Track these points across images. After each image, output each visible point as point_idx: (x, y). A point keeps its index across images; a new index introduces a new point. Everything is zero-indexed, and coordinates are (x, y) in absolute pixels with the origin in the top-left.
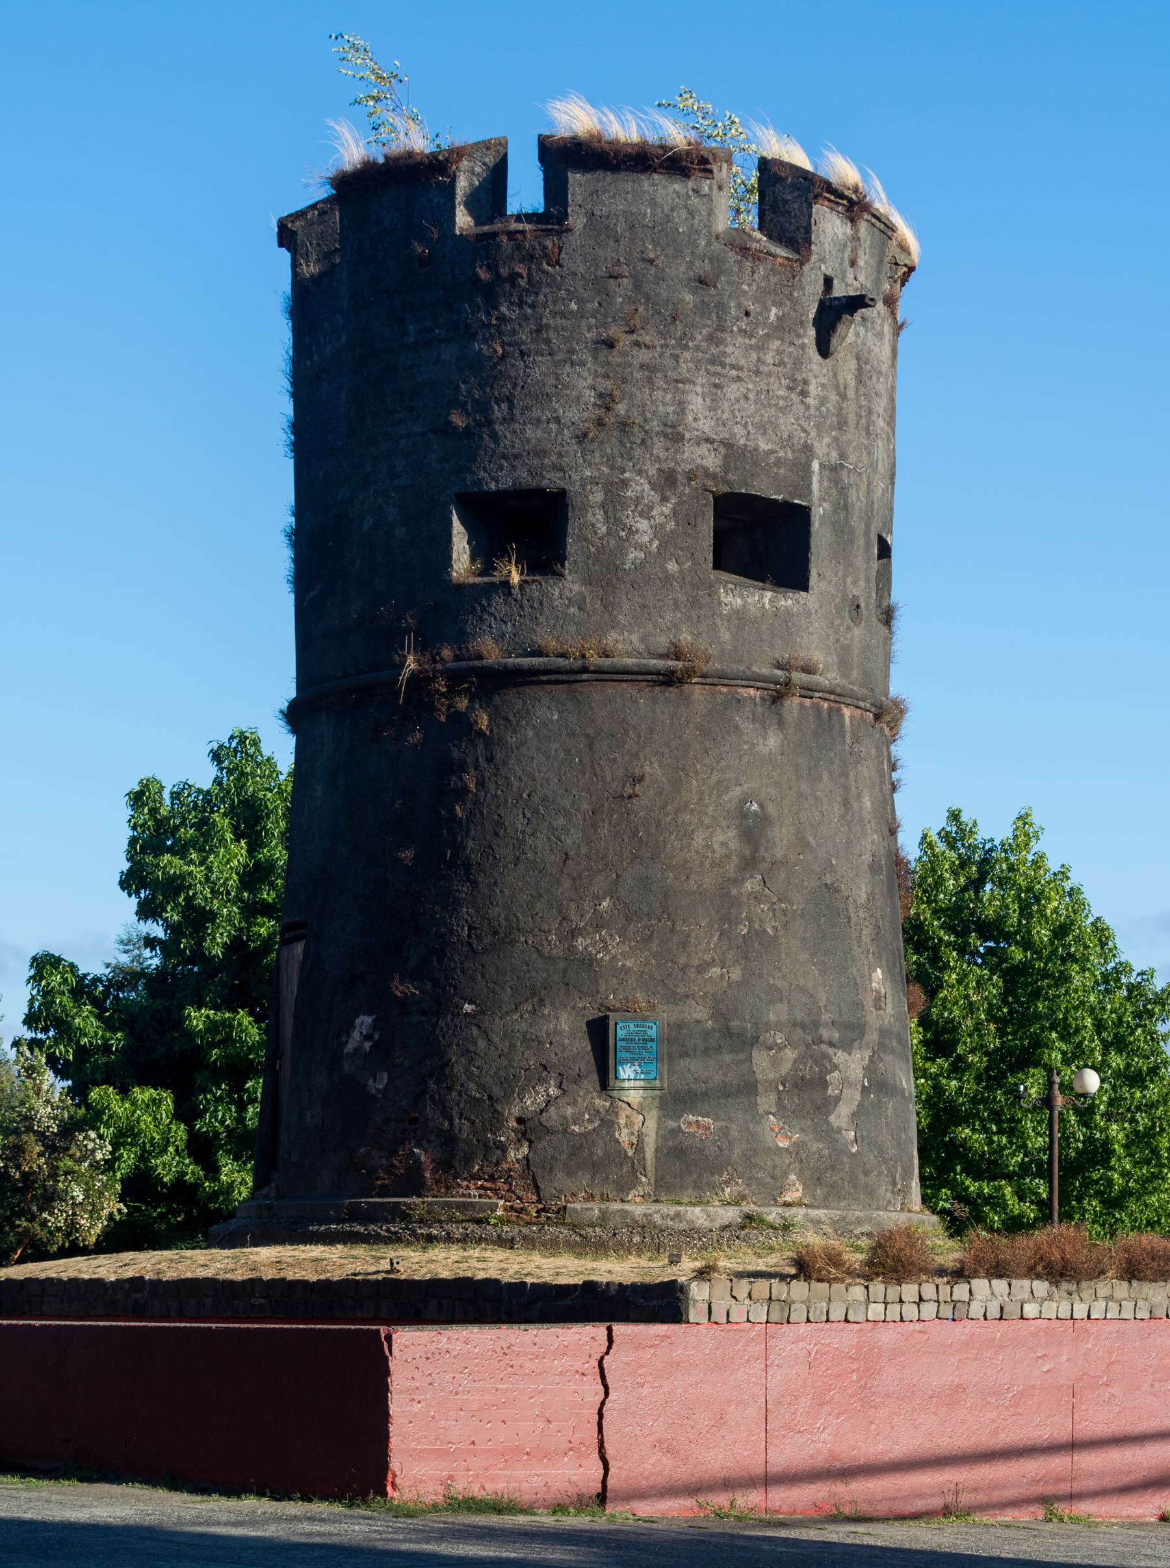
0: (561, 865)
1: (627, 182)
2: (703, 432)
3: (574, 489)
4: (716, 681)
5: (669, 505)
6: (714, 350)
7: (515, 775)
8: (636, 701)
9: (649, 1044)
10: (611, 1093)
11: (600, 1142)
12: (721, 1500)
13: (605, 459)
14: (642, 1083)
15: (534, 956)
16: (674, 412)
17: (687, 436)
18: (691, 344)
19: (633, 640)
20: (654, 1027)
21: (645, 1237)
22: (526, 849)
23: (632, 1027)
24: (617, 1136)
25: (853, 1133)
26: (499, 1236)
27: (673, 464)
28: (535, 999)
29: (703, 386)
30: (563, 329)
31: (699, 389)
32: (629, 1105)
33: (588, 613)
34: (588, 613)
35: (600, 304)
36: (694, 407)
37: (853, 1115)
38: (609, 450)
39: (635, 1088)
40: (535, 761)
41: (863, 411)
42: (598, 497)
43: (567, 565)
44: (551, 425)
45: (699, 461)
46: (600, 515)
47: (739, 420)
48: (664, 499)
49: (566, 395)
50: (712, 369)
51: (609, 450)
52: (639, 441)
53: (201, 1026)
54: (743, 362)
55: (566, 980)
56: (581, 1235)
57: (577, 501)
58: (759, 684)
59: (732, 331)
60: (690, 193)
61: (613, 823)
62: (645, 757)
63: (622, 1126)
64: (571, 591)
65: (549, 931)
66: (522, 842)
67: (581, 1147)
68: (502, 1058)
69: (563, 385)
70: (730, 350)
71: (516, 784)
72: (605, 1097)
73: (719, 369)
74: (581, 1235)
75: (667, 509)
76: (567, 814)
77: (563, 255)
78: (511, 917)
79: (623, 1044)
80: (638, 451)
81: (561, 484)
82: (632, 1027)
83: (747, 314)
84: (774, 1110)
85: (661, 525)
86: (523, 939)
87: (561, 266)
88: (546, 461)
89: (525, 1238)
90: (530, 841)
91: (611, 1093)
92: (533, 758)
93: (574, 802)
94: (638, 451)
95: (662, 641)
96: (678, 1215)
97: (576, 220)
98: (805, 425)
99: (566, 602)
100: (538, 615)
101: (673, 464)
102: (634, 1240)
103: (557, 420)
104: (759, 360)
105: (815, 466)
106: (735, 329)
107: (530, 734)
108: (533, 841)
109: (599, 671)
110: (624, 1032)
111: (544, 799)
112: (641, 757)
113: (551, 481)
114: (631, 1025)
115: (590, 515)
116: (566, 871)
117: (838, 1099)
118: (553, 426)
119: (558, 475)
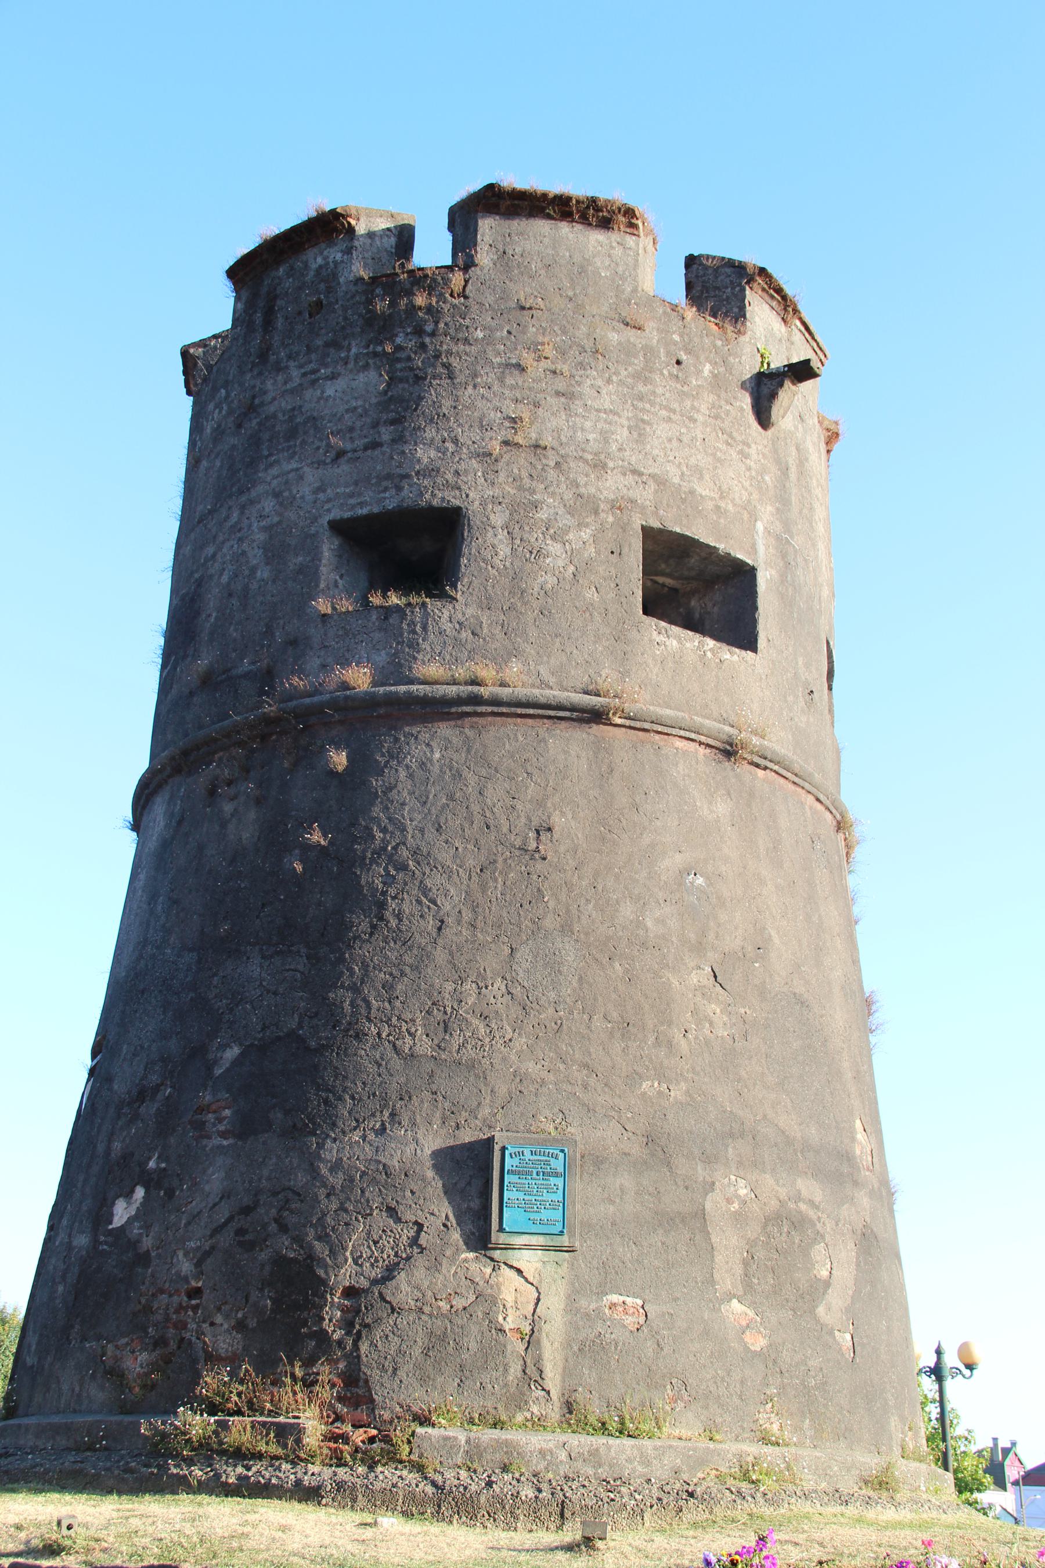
0: (434, 935)
1: (541, 226)
2: (629, 463)
3: (473, 505)
4: (647, 726)
5: (588, 531)
6: (641, 388)
7: (379, 826)
8: (544, 740)
9: (553, 1180)
10: (497, 1254)
11: (474, 1329)
12: (427, 688)
13: (511, 480)
14: (540, 1240)
15: (390, 1053)
16: (595, 440)
17: (611, 464)
18: (614, 378)
19: (542, 672)
20: (561, 1155)
21: (540, 1491)
22: (387, 914)
23: (528, 1155)
24: (500, 1319)
25: (848, 1337)
26: (298, 1483)
27: (593, 491)
28: (386, 1114)
29: (628, 419)
30: (466, 354)
31: (626, 423)
32: (519, 1271)
33: (484, 639)
34: (484, 639)
35: (509, 332)
36: (618, 437)
37: (848, 1310)
38: (516, 471)
39: (528, 1247)
40: (407, 808)
41: (597, 1403)
42: (499, 518)
43: (459, 586)
44: (447, 444)
45: (625, 491)
46: (502, 535)
47: (671, 458)
48: (581, 525)
49: (467, 415)
50: (640, 405)
51: (516, 471)
52: (552, 464)
53: (255, 1325)
54: (675, 406)
55: (434, 1087)
56: (434, 1484)
57: (476, 521)
58: (703, 739)
59: (662, 374)
60: (614, 244)
61: (508, 883)
62: (554, 805)
63: (508, 1305)
64: (464, 614)
65: (413, 1020)
66: (382, 905)
67: (443, 1338)
68: (332, 1198)
69: (464, 406)
70: (660, 391)
71: (379, 835)
72: (484, 1259)
73: (647, 406)
74: (434, 1484)
75: (586, 534)
76: (448, 873)
77: (469, 287)
78: (359, 1002)
79: (514, 1179)
80: (552, 474)
81: (457, 502)
82: (528, 1155)
83: (678, 363)
84: (741, 1293)
85: (578, 551)
86: (374, 1030)
87: (466, 297)
88: (439, 480)
89: (340, 1486)
90: (393, 905)
91: (490, 1253)
92: (403, 804)
93: (455, 856)
94: (552, 474)
95: (580, 677)
96: (594, 1453)
97: (484, 257)
98: (747, 484)
99: (457, 626)
100: (420, 641)
101: (593, 491)
102: (523, 1494)
103: (455, 441)
104: (693, 408)
105: (760, 526)
106: (665, 372)
107: (403, 774)
108: (398, 904)
109: (495, 702)
110: (516, 1161)
111: (416, 852)
112: (549, 805)
113: (412, 223)
114: (527, 1152)
115: (490, 534)
116: (440, 942)
117: (827, 1284)
118: (450, 445)
119: (453, 494)
